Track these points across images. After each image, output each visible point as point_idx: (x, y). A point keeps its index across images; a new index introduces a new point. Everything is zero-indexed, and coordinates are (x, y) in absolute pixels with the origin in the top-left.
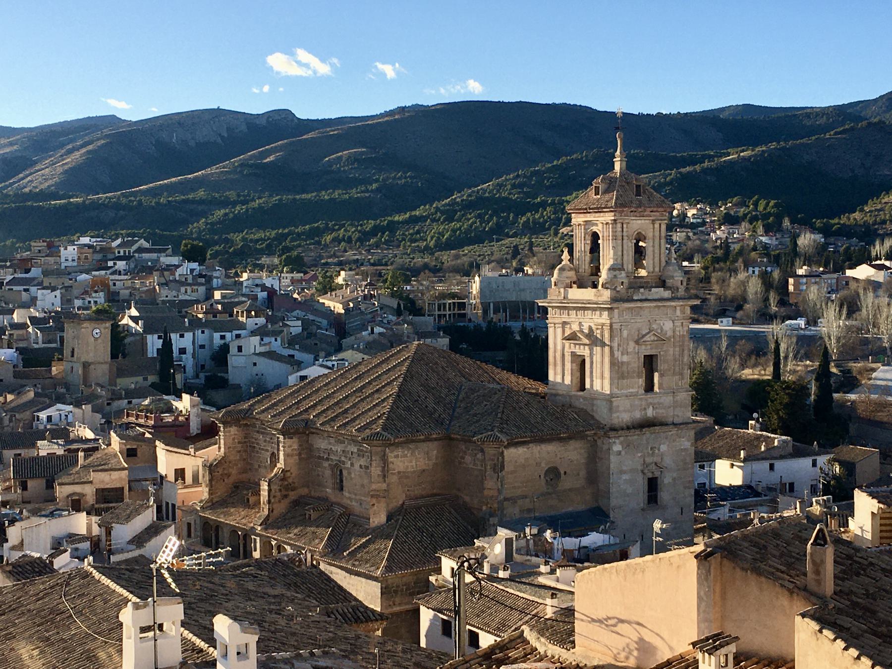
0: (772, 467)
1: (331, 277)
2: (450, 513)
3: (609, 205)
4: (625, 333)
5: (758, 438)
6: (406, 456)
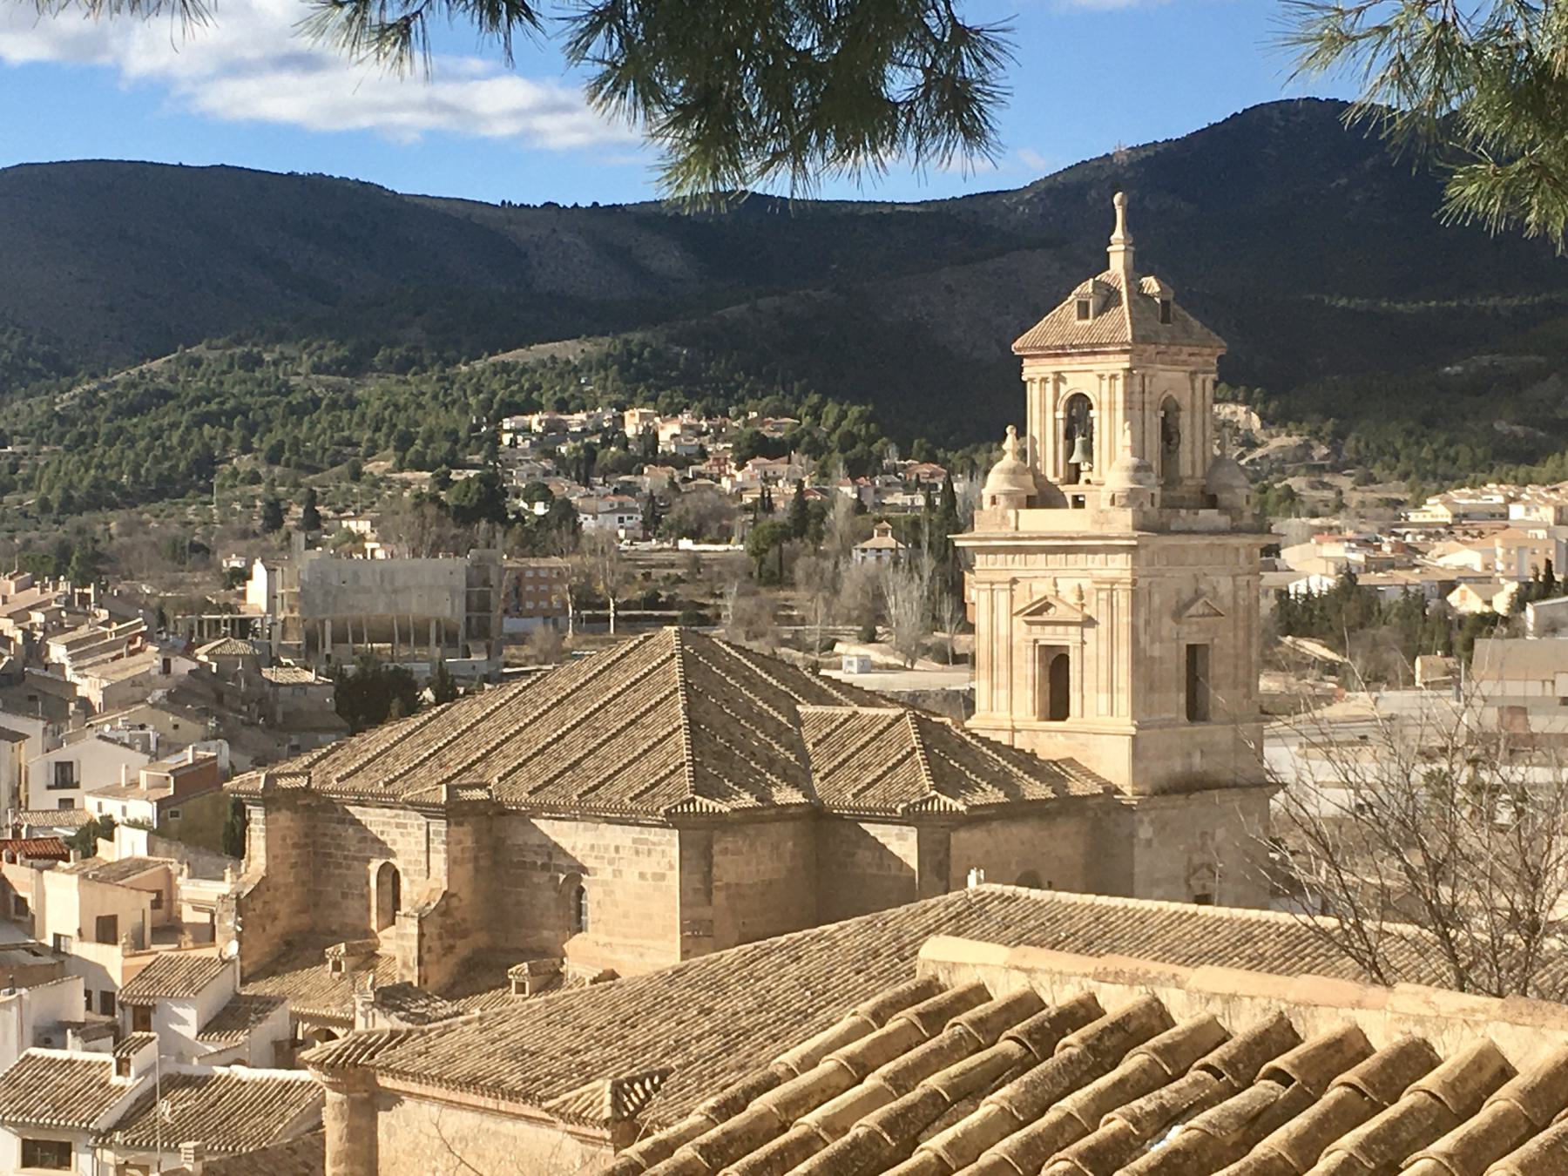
4: (1157, 599)
6: (738, 852)
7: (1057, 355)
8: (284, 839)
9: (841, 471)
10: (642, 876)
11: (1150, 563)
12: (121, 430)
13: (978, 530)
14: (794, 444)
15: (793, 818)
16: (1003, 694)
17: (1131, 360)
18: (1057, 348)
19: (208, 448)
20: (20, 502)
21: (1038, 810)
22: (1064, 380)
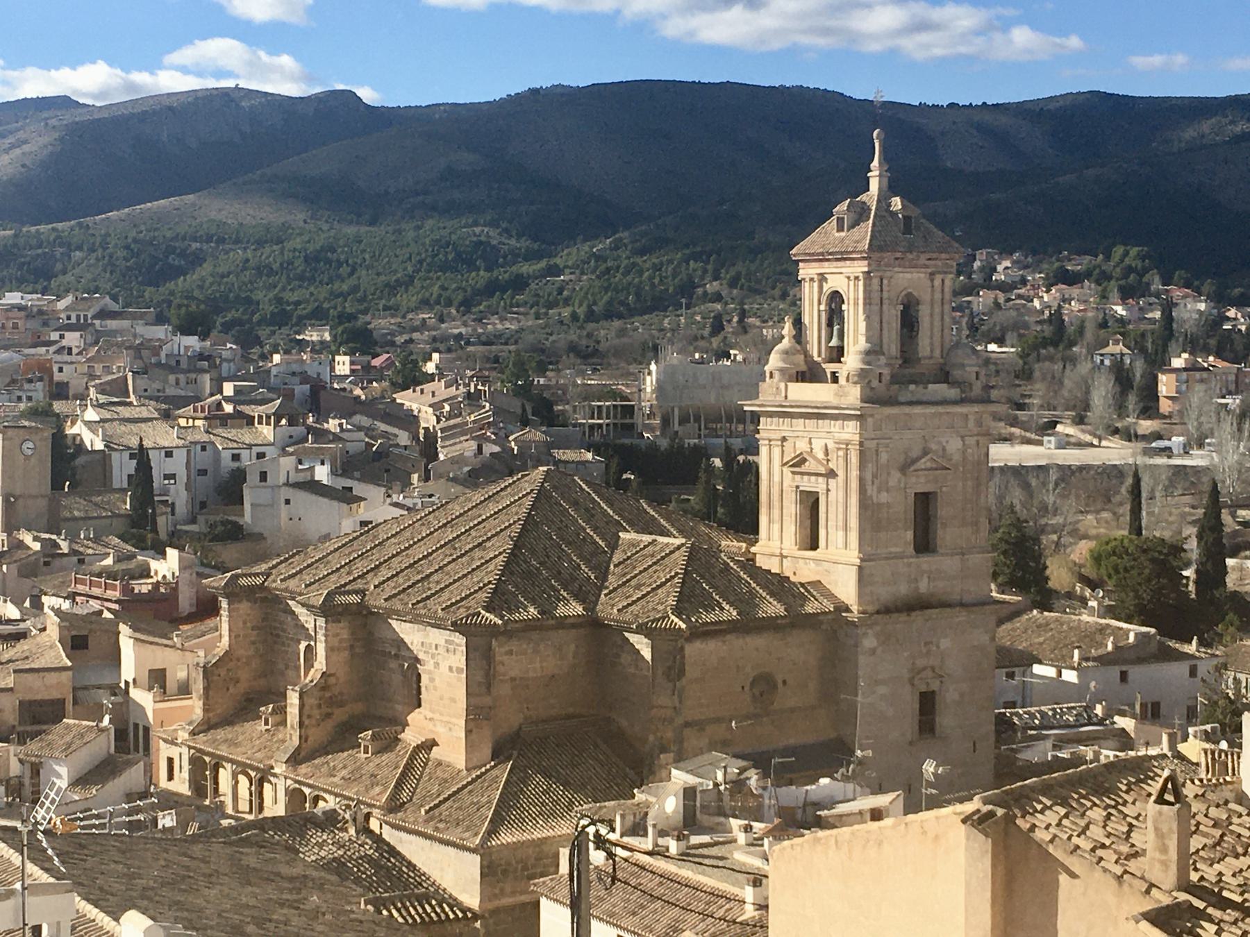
0: (1124, 676)
1: (415, 362)
2: (596, 746)
3: (860, 247)
4: (884, 457)
5: (1102, 630)
7: (821, 260)
8: (245, 623)
9: (1115, 295)
10: (451, 669)
11: (877, 428)
12: (634, 264)
14: (1088, 275)
15: (573, 626)
16: (776, 527)
17: (869, 265)
18: (819, 254)
19: (690, 278)
20: (560, 314)
21: (771, 625)
22: (826, 280)
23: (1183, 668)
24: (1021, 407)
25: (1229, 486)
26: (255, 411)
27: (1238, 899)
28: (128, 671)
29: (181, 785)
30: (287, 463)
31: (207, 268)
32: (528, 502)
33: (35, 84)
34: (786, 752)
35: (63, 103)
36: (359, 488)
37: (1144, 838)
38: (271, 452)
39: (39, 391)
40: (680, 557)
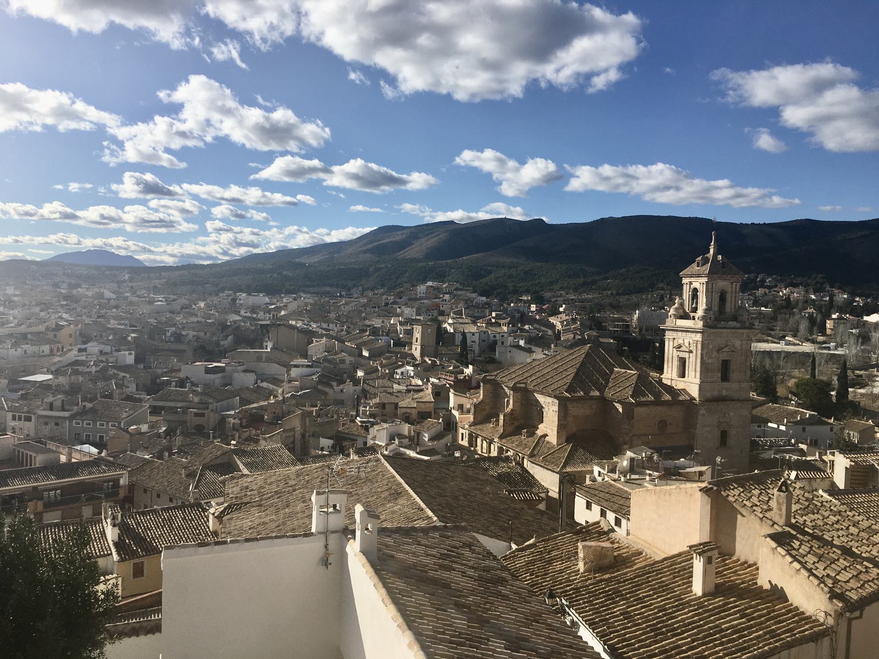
0: (804, 429)
4: (711, 347)
5: (796, 412)
13: (667, 324)
14: (801, 284)
21: (666, 403)
23: (828, 427)
24: (772, 330)
25: (851, 362)
26: (502, 322)
27: (811, 532)
28: (451, 405)
29: (465, 443)
30: (510, 339)
31: (493, 275)
32: (583, 356)
33: (441, 217)
34: (667, 448)
35: (451, 223)
36: (534, 348)
37: (773, 504)
38: (506, 335)
39: (435, 313)
40: (635, 378)
